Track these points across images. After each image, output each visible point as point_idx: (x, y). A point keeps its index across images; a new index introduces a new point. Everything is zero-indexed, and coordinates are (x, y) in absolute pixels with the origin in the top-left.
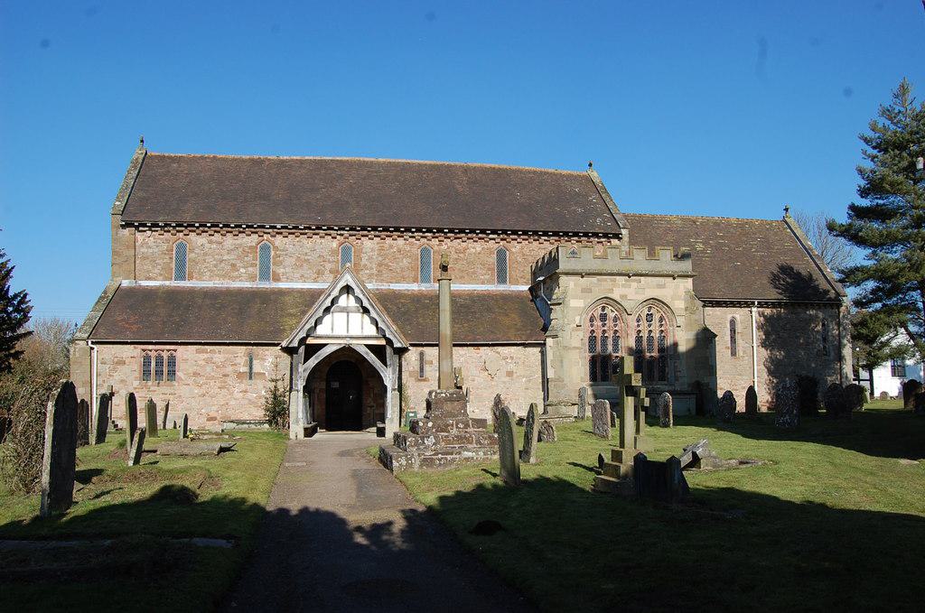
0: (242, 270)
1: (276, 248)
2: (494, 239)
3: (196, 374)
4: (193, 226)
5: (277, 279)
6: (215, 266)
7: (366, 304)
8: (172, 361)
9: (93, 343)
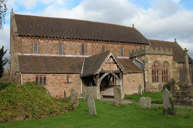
0: (54, 51)
1: (64, 45)
2: (120, 44)
4: (40, 37)
5: (64, 54)
6: (46, 49)
7: (116, 61)
8: (45, 79)
9: (21, 73)
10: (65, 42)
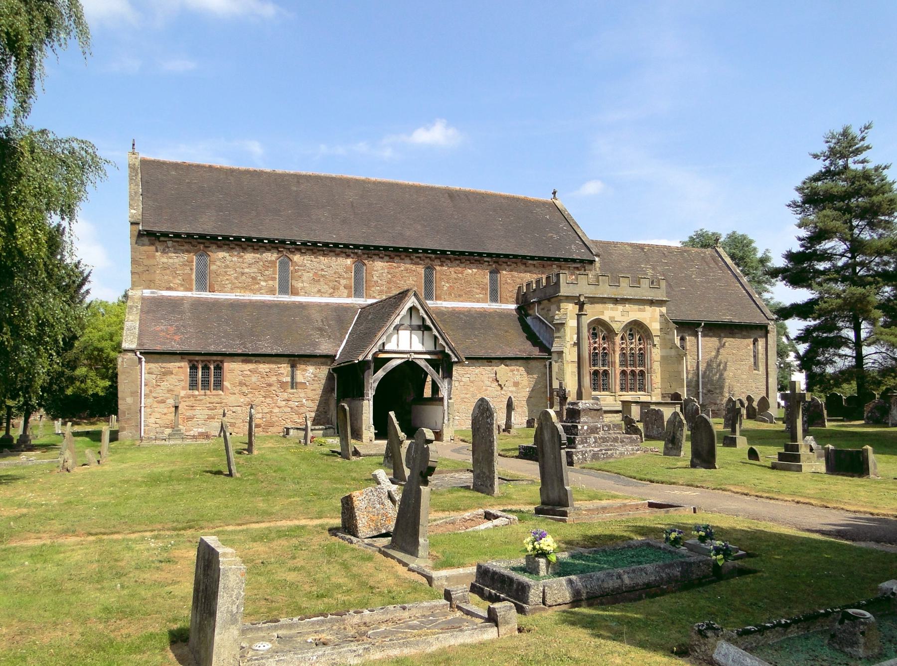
0: (263, 283)
3: (241, 384)
5: (295, 292)
6: (236, 278)
10: (297, 258)
